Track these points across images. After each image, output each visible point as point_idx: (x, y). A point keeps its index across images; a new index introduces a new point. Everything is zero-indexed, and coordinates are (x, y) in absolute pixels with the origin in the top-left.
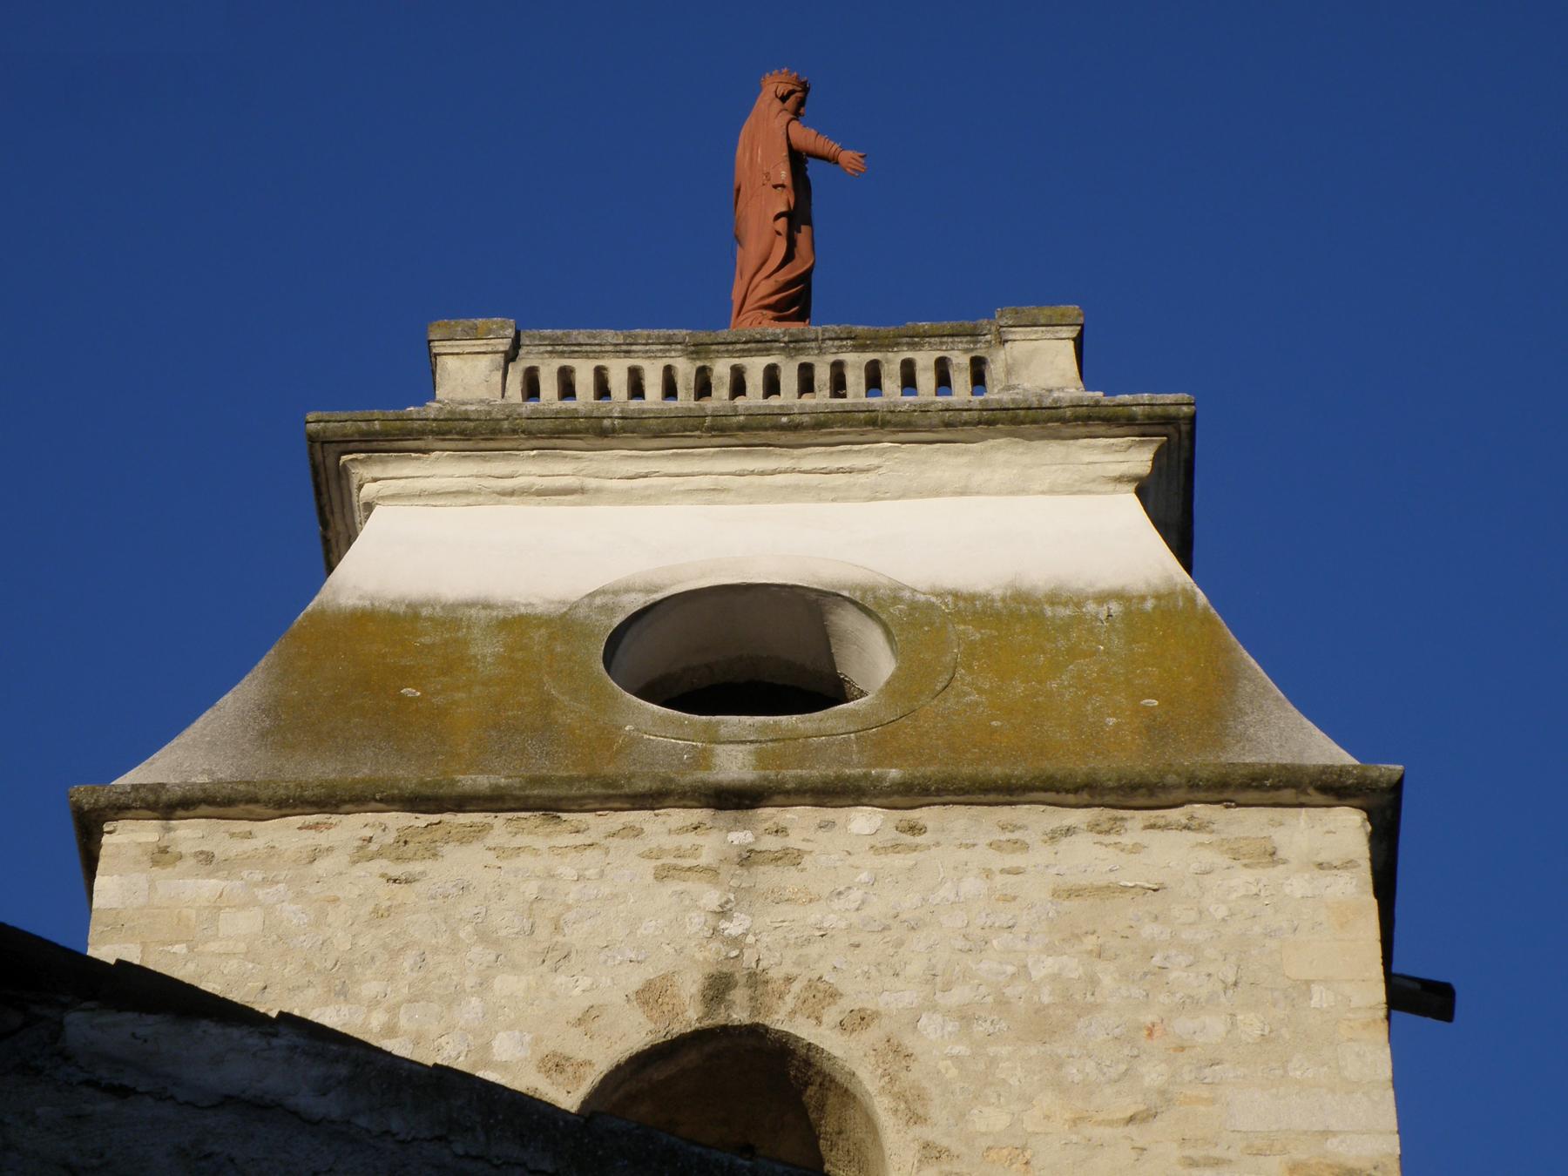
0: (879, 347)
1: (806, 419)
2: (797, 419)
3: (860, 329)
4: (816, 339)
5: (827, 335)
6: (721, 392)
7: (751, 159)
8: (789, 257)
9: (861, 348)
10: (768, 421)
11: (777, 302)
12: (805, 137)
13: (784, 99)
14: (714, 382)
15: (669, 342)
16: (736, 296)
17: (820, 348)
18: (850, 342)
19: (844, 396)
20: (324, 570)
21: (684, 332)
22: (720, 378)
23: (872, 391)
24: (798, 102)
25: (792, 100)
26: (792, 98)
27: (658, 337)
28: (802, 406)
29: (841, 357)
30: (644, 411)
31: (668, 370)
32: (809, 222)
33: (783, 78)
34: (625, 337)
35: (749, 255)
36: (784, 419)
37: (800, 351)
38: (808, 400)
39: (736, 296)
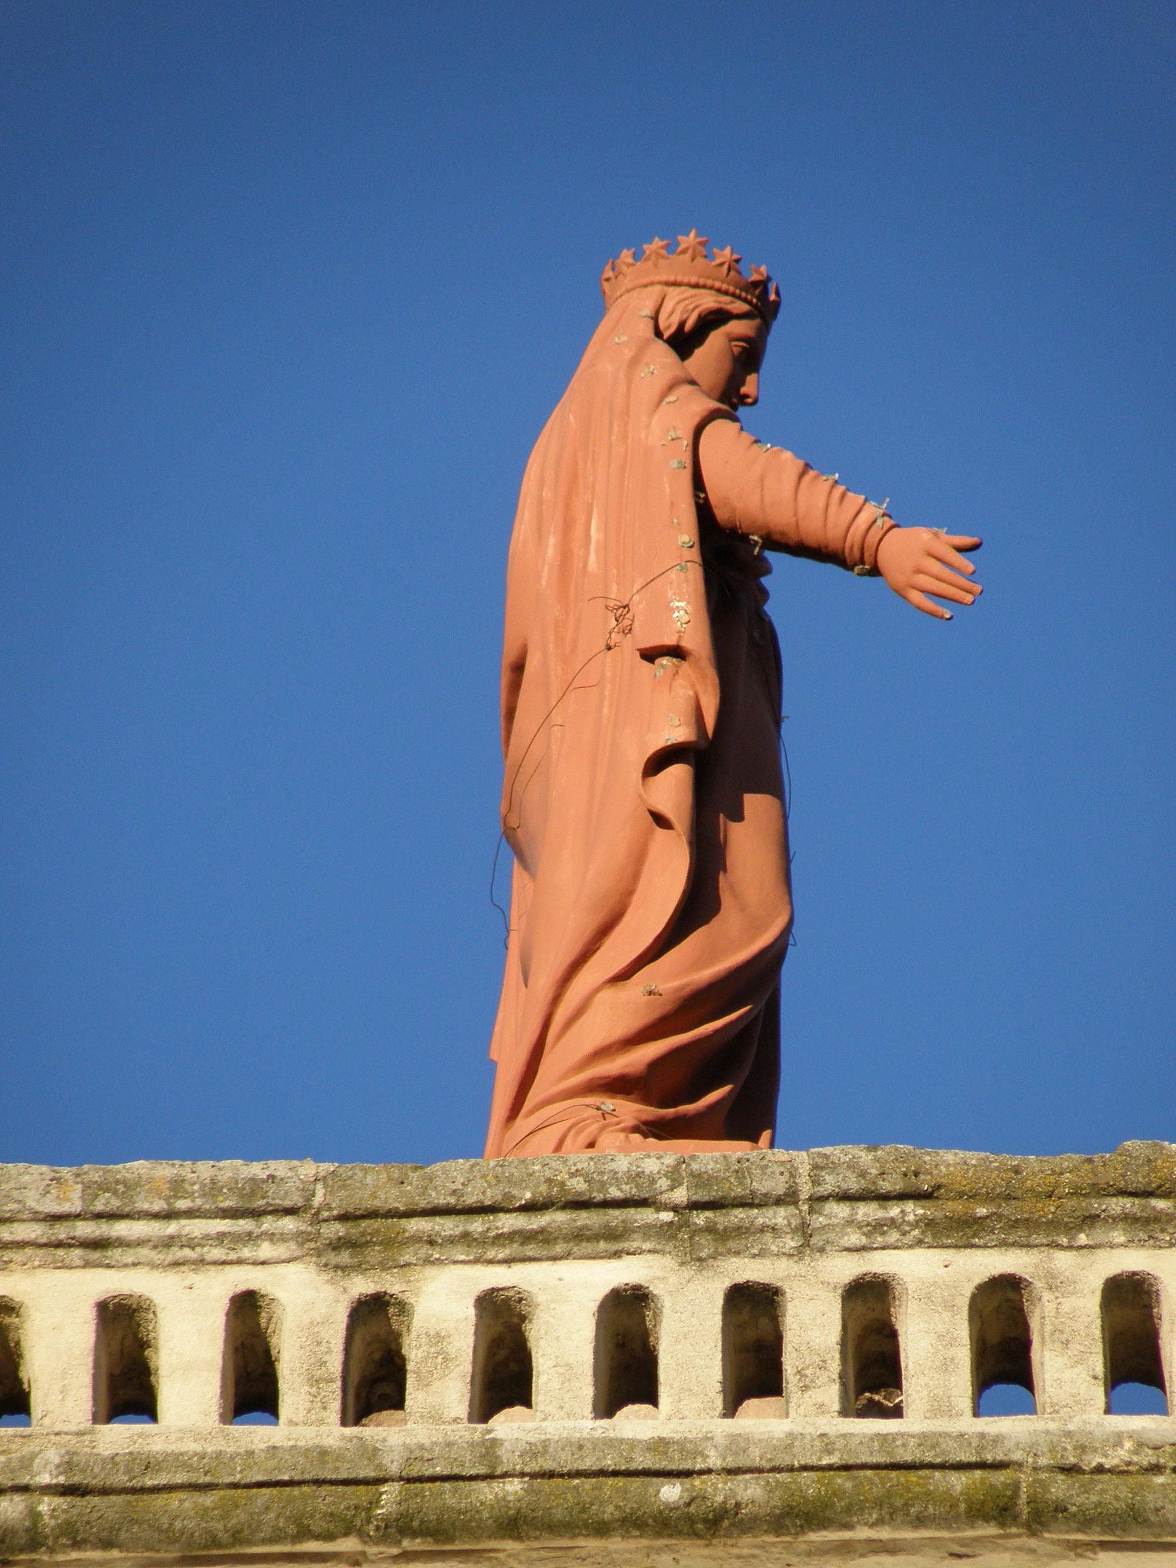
0: (1021, 1229)
1: (750, 1491)
2: (719, 1491)
3: (949, 1162)
4: (789, 1198)
5: (830, 1182)
6: (440, 1390)
7: (565, 556)
8: (697, 907)
9: (960, 1231)
10: (611, 1498)
11: (656, 1065)
12: (758, 478)
13: (684, 342)
14: (414, 1352)
15: (251, 1208)
16: (508, 1050)
17: (804, 1231)
18: (913, 1210)
19: (897, 1412)
20: (1023, 1391)
21: (308, 1169)
22: (438, 1338)
23: (1000, 1391)
24: (735, 349)
25: (713, 351)
26: (716, 340)
27: (213, 1188)
28: (736, 1443)
29: (880, 1263)
30: (149, 1464)
31: (247, 1308)
32: (772, 785)
33: (681, 266)
34: (91, 1190)
35: (554, 899)
36: (671, 1492)
37: (728, 1240)
38: (760, 1421)
39: (508, 1050)
